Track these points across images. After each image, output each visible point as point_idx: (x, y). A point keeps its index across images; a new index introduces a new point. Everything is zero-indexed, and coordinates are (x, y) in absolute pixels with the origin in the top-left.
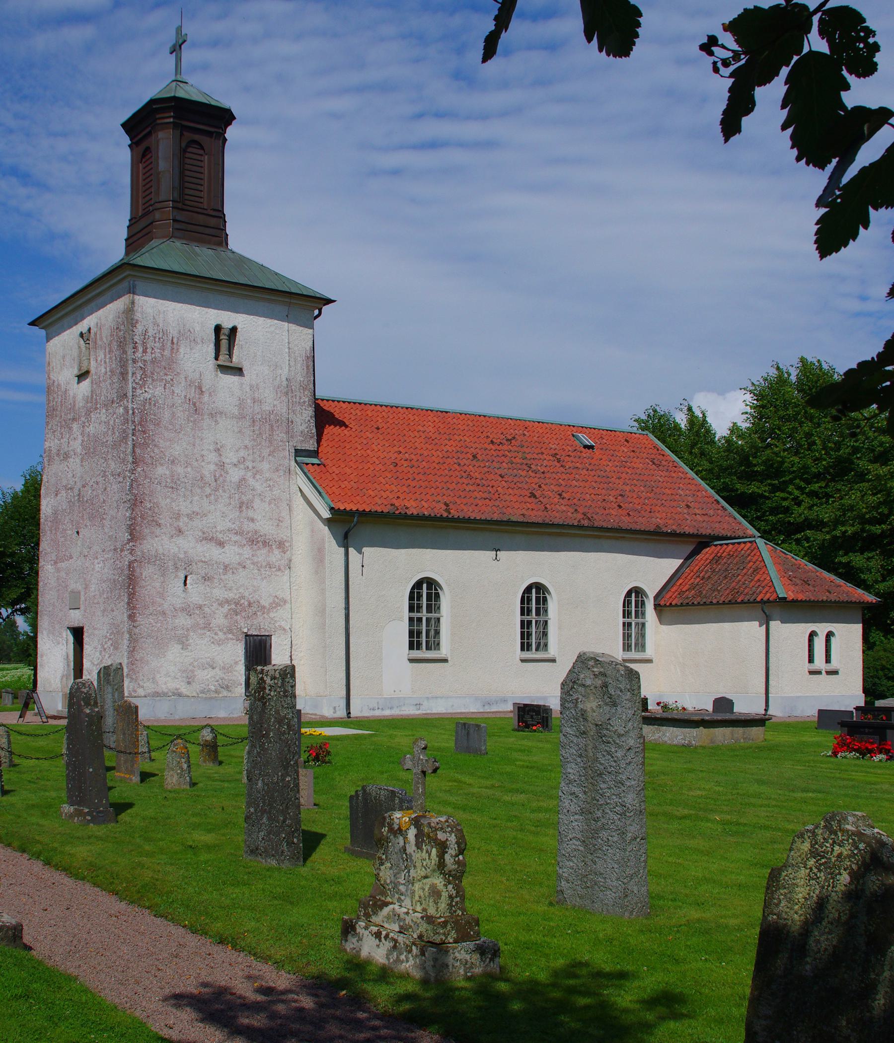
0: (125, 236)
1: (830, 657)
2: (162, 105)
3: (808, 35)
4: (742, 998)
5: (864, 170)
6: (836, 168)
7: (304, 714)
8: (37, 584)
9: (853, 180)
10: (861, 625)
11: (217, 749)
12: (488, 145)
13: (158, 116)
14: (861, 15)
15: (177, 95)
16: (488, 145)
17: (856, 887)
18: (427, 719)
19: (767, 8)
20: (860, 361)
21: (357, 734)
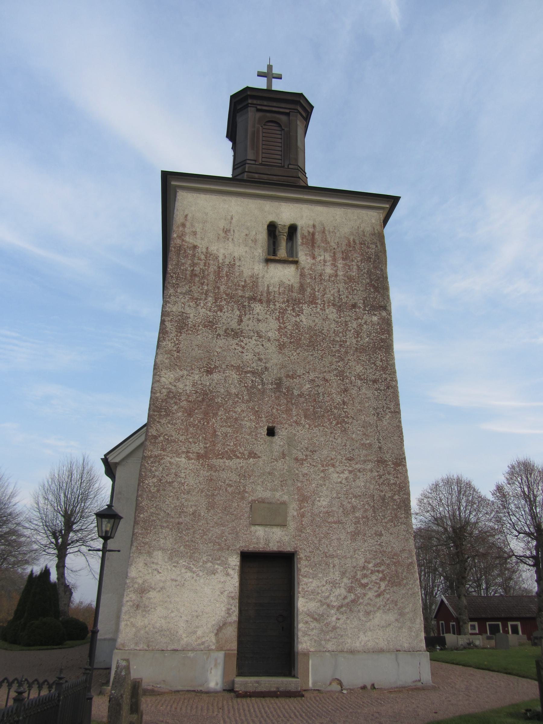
20: (466, 476)
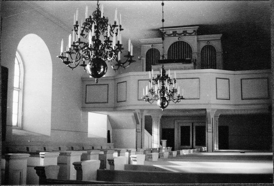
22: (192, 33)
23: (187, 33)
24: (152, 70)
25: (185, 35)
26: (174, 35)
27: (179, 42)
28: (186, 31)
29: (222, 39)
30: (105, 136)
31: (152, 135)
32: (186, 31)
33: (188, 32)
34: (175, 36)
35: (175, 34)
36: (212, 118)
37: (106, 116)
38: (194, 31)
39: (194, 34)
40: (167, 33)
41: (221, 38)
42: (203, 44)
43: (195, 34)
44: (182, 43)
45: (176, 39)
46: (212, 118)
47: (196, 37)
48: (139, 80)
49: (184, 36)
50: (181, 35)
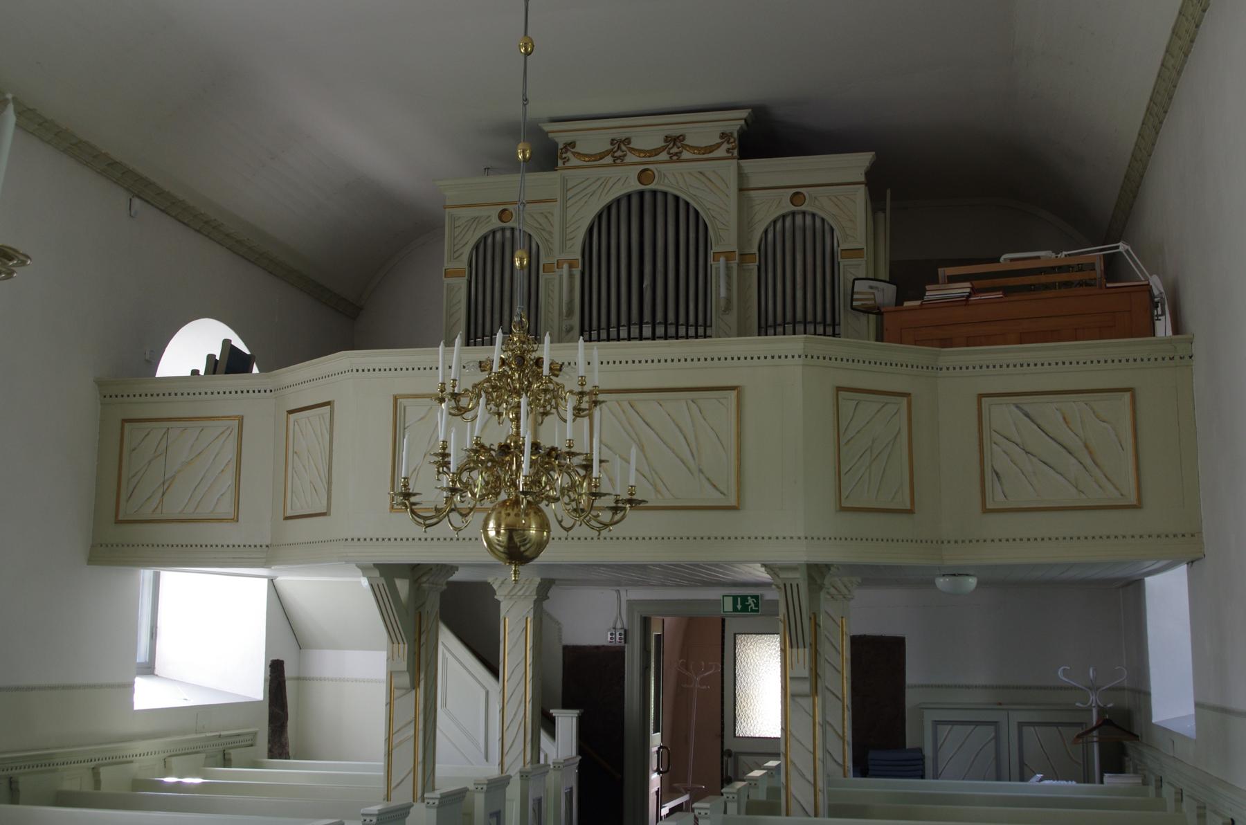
0: (509, 787)
1: (331, 498)
2: (653, 660)
3: (475, 514)
4: (777, 651)
5: (162, 781)
6: (370, 806)
7: (384, 650)
8: (269, 737)
9: (1094, 747)
10: (1154, 721)
11: (456, 393)
12: (804, 668)
13: (406, 645)
14: (865, 636)
15: (907, 690)
16: (804, 668)
17: (520, 546)
18: (873, 164)
19: (507, 789)
21: (1170, 314)
22: (710, 149)
23: (632, 150)
24: (547, 339)
25: (675, 158)
26: (671, 155)
27: (641, 194)
28: (627, 141)
29: (875, 182)
30: (254, 688)
31: (542, 708)
32: (627, 141)
33: (635, 144)
34: (619, 161)
35: (619, 149)
36: (383, 585)
37: (265, 581)
38: (725, 136)
39: (721, 152)
40: (578, 149)
41: (867, 174)
42: (768, 209)
43: (728, 151)
44: (660, 198)
45: (624, 181)
46: (383, 585)
47: (735, 162)
48: (981, 396)
49: (671, 161)
50: (602, 162)
